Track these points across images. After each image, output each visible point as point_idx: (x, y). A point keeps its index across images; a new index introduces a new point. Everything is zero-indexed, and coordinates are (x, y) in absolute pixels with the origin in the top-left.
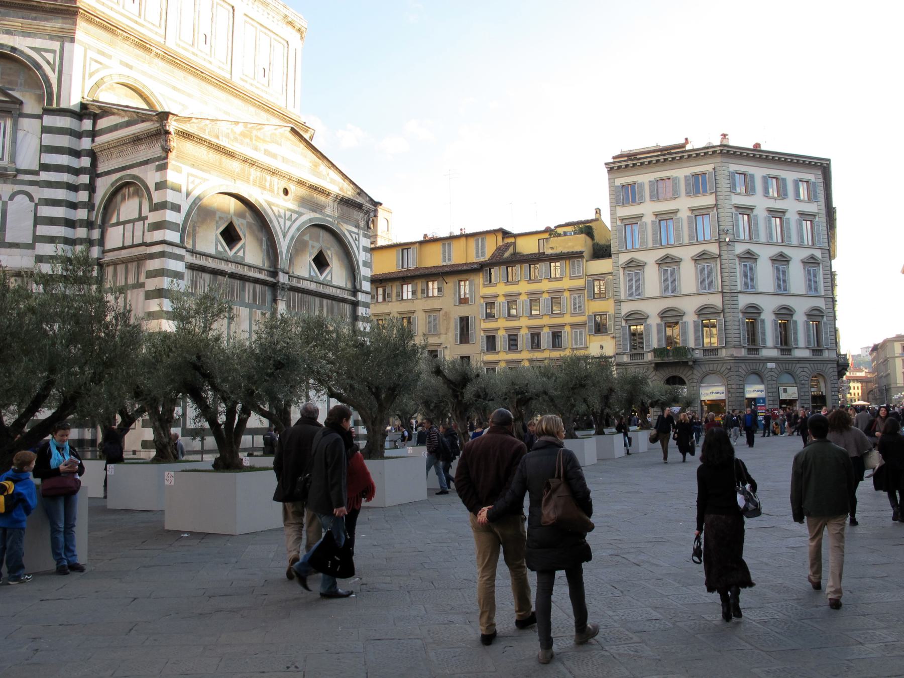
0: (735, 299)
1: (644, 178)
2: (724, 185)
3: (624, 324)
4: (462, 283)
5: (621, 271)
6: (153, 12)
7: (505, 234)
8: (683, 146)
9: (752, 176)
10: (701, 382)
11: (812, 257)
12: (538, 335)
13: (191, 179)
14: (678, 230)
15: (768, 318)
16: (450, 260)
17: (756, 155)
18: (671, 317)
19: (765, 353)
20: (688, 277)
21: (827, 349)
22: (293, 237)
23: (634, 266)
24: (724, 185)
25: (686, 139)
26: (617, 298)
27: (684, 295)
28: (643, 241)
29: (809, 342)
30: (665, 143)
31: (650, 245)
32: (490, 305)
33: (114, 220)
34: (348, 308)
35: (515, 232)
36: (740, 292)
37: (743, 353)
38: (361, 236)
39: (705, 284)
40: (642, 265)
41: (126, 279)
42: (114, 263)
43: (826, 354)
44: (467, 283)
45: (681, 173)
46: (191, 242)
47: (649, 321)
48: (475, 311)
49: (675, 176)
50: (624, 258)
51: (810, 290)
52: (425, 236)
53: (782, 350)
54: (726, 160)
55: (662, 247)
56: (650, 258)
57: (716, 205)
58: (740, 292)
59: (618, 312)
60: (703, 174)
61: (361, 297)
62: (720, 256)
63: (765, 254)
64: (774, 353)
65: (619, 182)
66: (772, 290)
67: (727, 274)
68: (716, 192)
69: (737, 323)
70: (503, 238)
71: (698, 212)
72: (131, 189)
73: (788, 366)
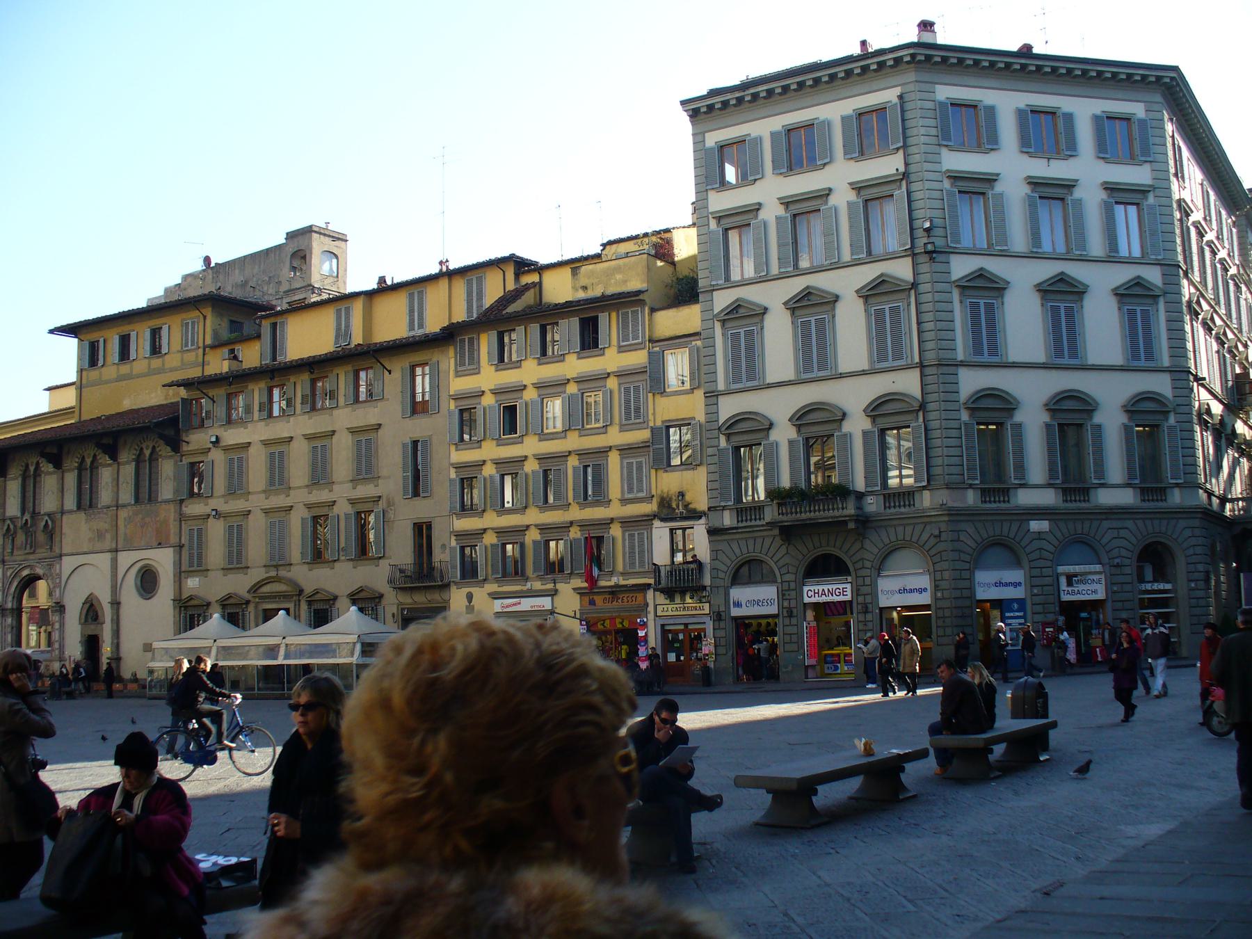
0: (951, 379)
1: (763, 127)
2: (923, 130)
3: (723, 442)
5: (718, 326)
7: (521, 265)
9: (991, 111)
10: (879, 570)
11: (1138, 282)
14: (831, 235)
15: (1032, 419)
16: (421, 326)
17: (1023, 66)
18: (817, 425)
19: (1025, 498)
20: (851, 333)
21: (1177, 485)
23: (743, 317)
24: (923, 130)
26: (711, 387)
27: (841, 376)
29: (1130, 469)
31: (775, 270)
35: (543, 260)
36: (963, 364)
37: (971, 498)
39: (885, 352)
43: (1176, 498)
44: (427, 369)
50: (722, 300)
52: (382, 280)
54: (926, 77)
55: (798, 272)
56: (774, 297)
57: (905, 175)
58: (963, 364)
62: (914, 285)
65: (712, 139)
66: (1041, 357)
68: (905, 146)
69: (954, 433)
70: (517, 276)
71: (870, 195)
73: (1079, 526)
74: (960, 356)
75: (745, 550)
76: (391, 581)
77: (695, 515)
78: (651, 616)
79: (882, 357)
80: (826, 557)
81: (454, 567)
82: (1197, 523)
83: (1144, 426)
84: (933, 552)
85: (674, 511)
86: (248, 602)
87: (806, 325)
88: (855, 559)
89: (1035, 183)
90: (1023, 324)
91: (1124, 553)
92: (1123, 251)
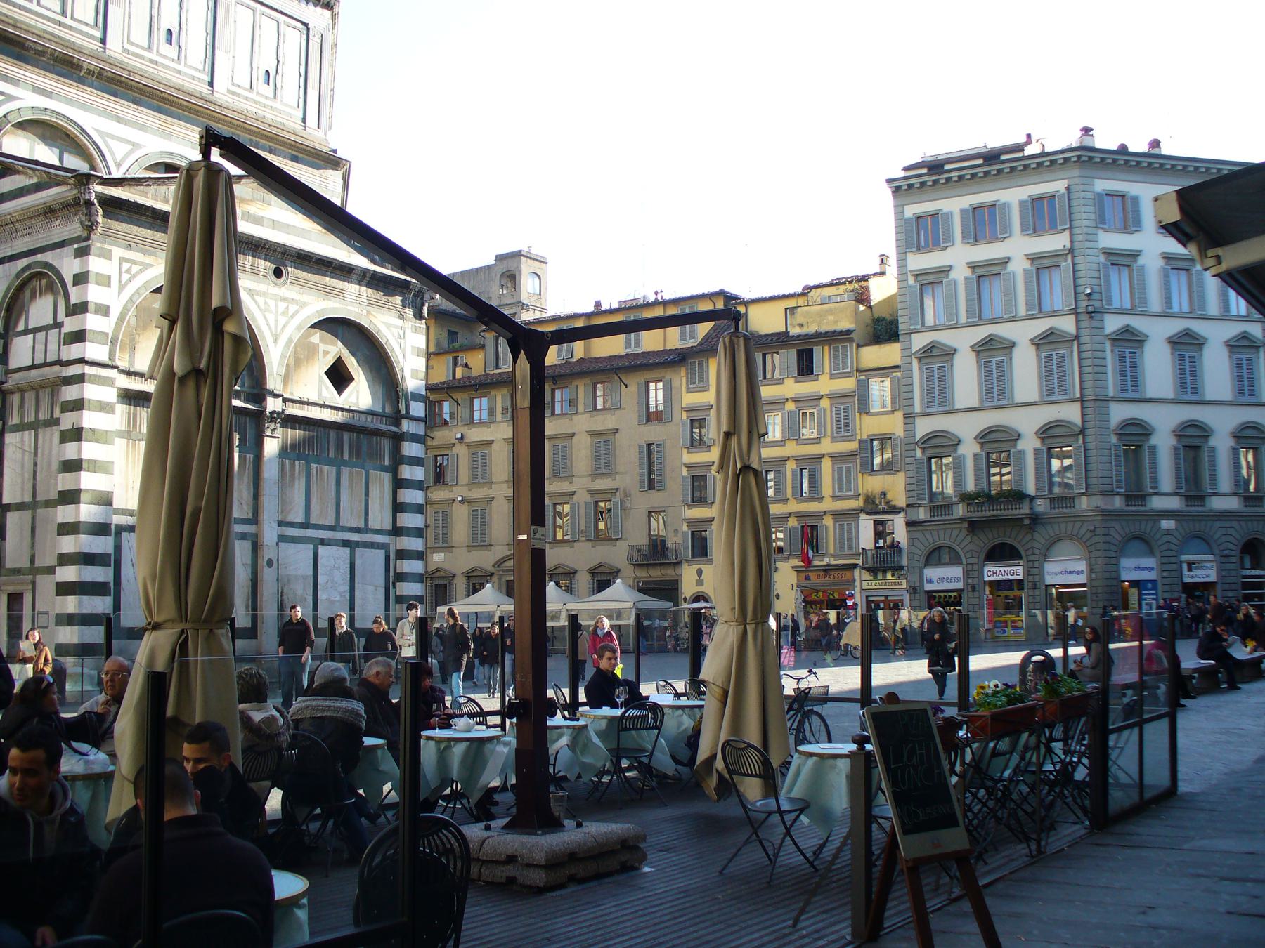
0: (1103, 411)
1: (954, 205)
2: (1084, 216)
3: (919, 454)
4: (652, 386)
6: (85, 7)
8: (1019, 148)
9: (1136, 200)
12: (703, 478)
13: (126, 266)
14: (1009, 294)
15: (1163, 442)
18: (998, 443)
19: (1157, 503)
20: (1025, 372)
22: (290, 340)
23: (937, 355)
24: (1084, 216)
25: (1029, 136)
26: (908, 410)
27: (1017, 405)
28: (952, 311)
30: (996, 141)
32: (698, 422)
33: (21, 327)
34: (386, 443)
36: (1113, 399)
37: (1118, 503)
38: (408, 332)
39: (1052, 388)
41: (37, 412)
42: (22, 391)
44: (660, 385)
45: (1013, 196)
46: (127, 357)
47: (961, 450)
48: (671, 434)
49: (1003, 200)
50: (919, 341)
51: (1241, 394)
52: (598, 304)
53: (1188, 498)
56: (963, 340)
57: (1071, 250)
58: (1113, 399)
59: (910, 432)
60: (1051, 197)
61: (406, 426)
62: (1077, 337)
63: (1158, 332)
64: (1174, 503)
65: (911, 211)
66: (1170, 395)
67: (1089, 369)
68: (1071, 228)
69: (1106, 452)
71: (1042, 264)
72: (44, 282)
74: (1111, 393)
75: (931, 540)
77: (895, 510)
78: (858, 589)
85: (876, 506)
86: (492, 574)
90: (1158, 368)
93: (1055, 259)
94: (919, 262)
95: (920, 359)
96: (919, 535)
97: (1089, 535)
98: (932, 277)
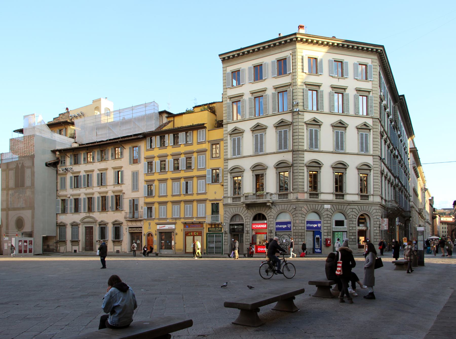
4: (117, 149)
20: (352, 139)
23: (237, 132)
26: (226, 157)
31: (247, 117)
35: (175, 112)
36: (306, 151)
40: (242, 132)
49: (242, 68)
50: (230, 127)
56: (247, 126)
58: (306, 151)
63: (327, 121)
64: (331, 197)
66: (331, 149)
74: (305, 148)
75: (234, 211)
76: (125, 218)
79: (280, 147)
80: (260, 214)
81: (145, 214)
82: (378, 208)
83: (363, 174)
84: (293, 214)
87: (257, 136)
88: (268, 215)
89: (333, 87)
90: (327, 137)
91: (354, 217)
92: (361, 113)
93: (285, 88)
94: (232, 92)
95: (231, 134)
96: (228, 209)
97: (293, 210)
98: (236, 98)
